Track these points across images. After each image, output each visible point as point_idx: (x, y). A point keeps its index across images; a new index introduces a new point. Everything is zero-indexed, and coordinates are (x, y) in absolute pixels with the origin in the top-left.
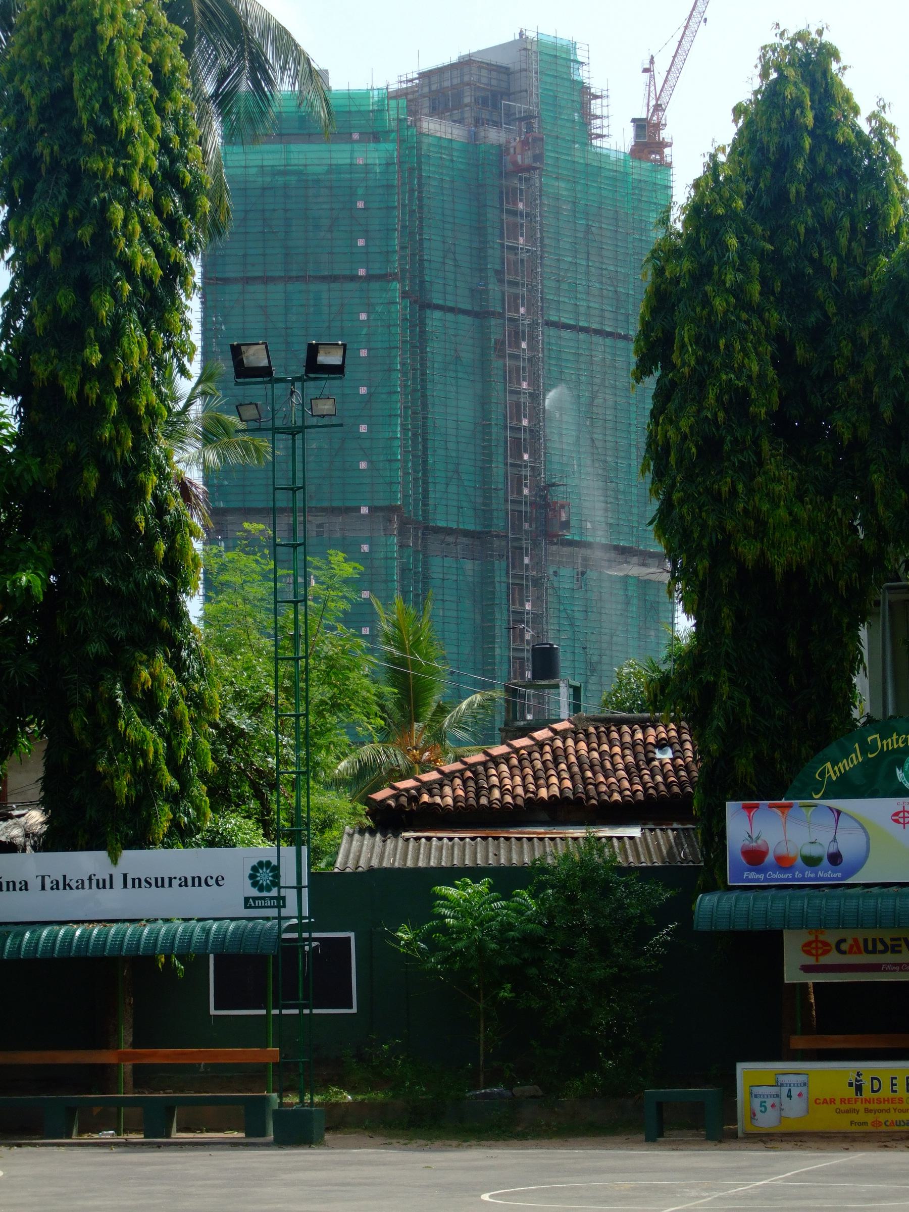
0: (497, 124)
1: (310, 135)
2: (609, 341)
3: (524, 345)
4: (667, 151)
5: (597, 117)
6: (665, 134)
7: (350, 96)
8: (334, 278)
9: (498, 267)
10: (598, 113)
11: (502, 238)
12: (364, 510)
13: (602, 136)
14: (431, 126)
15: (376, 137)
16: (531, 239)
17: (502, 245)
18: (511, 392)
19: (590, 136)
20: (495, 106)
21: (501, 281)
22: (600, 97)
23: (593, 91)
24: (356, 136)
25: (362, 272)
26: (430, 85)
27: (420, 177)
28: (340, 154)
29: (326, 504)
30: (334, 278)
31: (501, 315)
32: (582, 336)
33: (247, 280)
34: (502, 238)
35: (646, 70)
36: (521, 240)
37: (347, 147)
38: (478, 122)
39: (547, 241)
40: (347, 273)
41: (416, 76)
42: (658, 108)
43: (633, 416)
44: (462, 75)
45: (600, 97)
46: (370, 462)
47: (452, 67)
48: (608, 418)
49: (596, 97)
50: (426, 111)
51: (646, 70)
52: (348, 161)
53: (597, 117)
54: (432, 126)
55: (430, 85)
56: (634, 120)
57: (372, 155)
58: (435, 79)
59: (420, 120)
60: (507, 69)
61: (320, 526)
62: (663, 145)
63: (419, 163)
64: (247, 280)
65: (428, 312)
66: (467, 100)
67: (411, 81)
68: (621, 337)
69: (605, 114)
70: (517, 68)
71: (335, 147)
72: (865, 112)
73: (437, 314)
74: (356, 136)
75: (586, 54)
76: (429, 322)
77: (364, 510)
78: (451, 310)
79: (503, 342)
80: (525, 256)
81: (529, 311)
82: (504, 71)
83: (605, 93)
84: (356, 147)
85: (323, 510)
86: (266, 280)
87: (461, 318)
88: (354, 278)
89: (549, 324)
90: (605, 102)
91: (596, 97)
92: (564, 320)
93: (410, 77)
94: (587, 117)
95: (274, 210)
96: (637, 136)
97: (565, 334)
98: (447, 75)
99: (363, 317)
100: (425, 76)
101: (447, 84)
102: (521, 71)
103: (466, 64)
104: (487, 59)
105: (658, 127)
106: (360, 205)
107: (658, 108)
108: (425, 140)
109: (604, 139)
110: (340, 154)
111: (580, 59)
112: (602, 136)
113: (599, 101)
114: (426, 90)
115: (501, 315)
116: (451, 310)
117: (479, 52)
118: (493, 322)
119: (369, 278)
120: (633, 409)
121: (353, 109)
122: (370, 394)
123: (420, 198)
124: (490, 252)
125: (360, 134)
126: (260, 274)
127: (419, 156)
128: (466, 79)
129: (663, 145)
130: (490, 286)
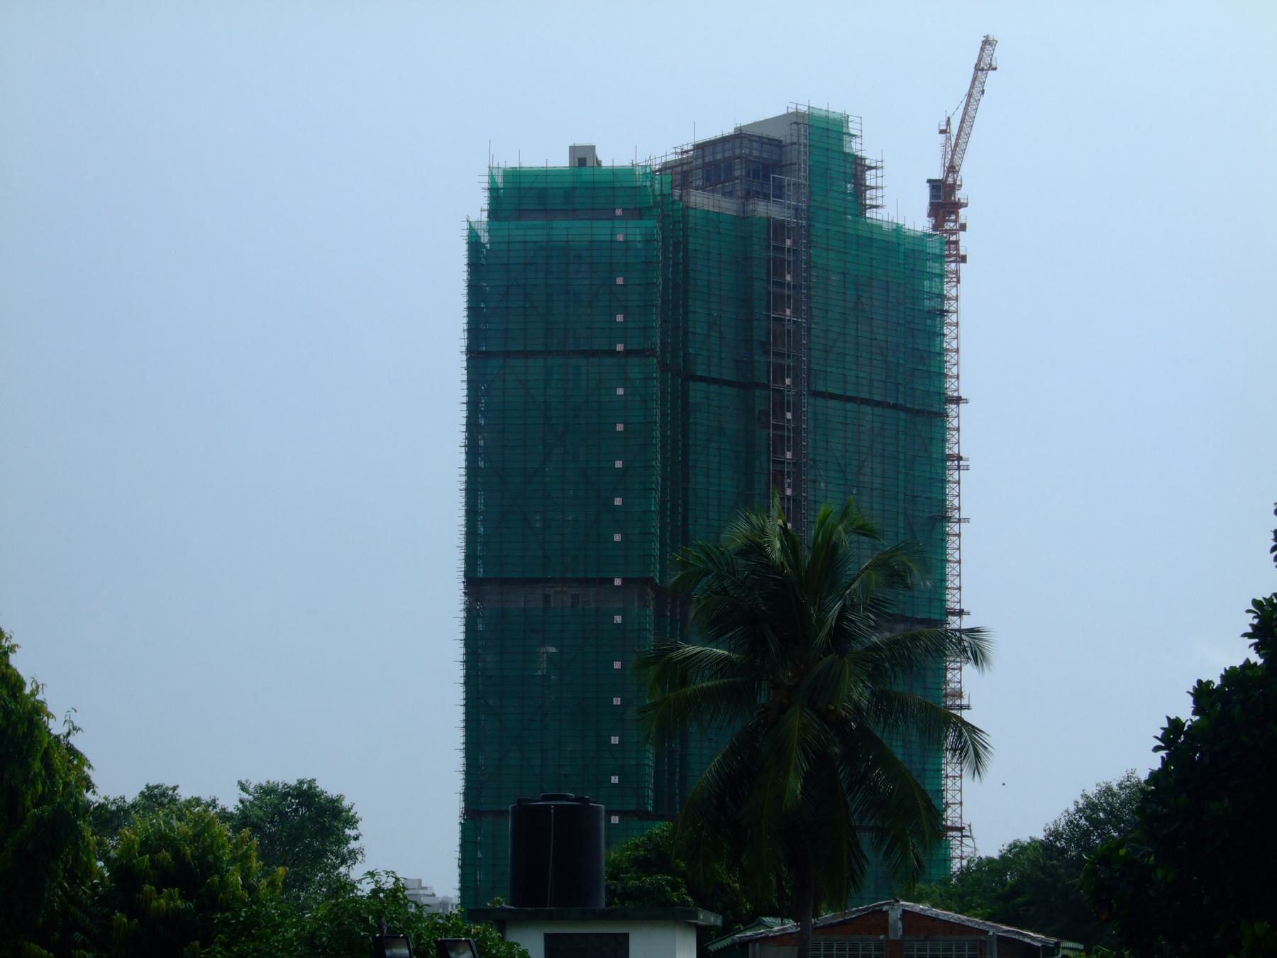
0: (766, 197)
1: (574, 210)
2: (878, 411)
3: (789, 416)
4: (962, 211)
5: (871, 188)
6: (960, 195)
7: (614, 172)
8: (594, 353)
9: (763, 339)
10: (873, 184)
11: (768, 310)
12: (618, 582)
13: (876, 207)
14: (700, 200)
15: (637, 213)
16: (796, 312)
17: (768, 317)
18: (775, 462)
19: (863, 208)
20: (766, 178)
21: (767, 353)
22: (875, 168)
23: (867, 162)
24: (619, 212)
25: (620, 348)
26: (703, 157)
27: (686, 251)
28: (601, 230)
29: (581, 575)
30: (594, 353)
31: (766, 387)
32: (850, 406)
33: (508, 354)
34: (768, 310)
35: (942, 132)
36: (788, 312)
37: (608, 224)
38: (748, 195)
39: (815, 312)
40: (606, 348)
41: (690, 147)
42: (952, 169)
43: (901, 483)
44: (733, 149)
45: (875, 168)
46: (624, 535)
47: (724, 140)
48: (875, 486)
49: (870, 168)
50: (699, 183)
51: (942, 132)
52: (608, 238)
53: (871, 188)
54: (699, 200)
55: (703, 157)
56: (929, 181)
57: (627, 232)
58: (708, 151)
59: (688, 194)
60: (780, 141)
61: (575, 597)
62: (959, 205)
63: (686, 236)
64: (508, 354)
65: (692, 384)
66: (737, 173)
67: (687, 152)
68: (888, 406)
69: (879, 184)
70: (788, 141)
71: (596, 223)
72: (60, 717)
73: (702, 386)
74: (619, 212)
75: (858, 127)
76: (691, 393)
77: (618, 582)
78: (715, 381)
79: (768, 414)
80: (792, 327)
81: (794, 381)
82: (777, 144)
83: (879, 164)
84: (617, 223)
85: (579, 580)
86: (527, 354)
87: (726, 389)
88: (613, 353)
89: (816, 394)
90: (879, 173)
91: (870, 168)
92: (830, 390)
93: (685, 148)
94: (861, 188)
95: (535, 285)
96: (933, 196)
97: (831, 403)
98: (719, 148)
99: (620, 391)
100: (700, 147)
101: (719, 156)
102: (792, 144)
103: (740, 136)
104: (758, 132)
105: (953, 188)
106: (620, 281)
107: (952, 169)
108: (691, 212)
109: (879, 210)
110: (601, 230)
111: (852, 132)
112: (876, 207)
113: (873, 171)
114: (700, 161)
115: (766, 387)
116: (715, 381)
117: (755, 124)
118: (758, 393)
119: (627, 353)
120: (901, 477)
121: (618, 185)
122: (625, 468)
123: (686, 271)
124: (756, 324)
125: (624, 210)
126: (520, 348)
127: (685, 229)
128: (737, 152)
129: (959, 205)
130: (756, 358)
